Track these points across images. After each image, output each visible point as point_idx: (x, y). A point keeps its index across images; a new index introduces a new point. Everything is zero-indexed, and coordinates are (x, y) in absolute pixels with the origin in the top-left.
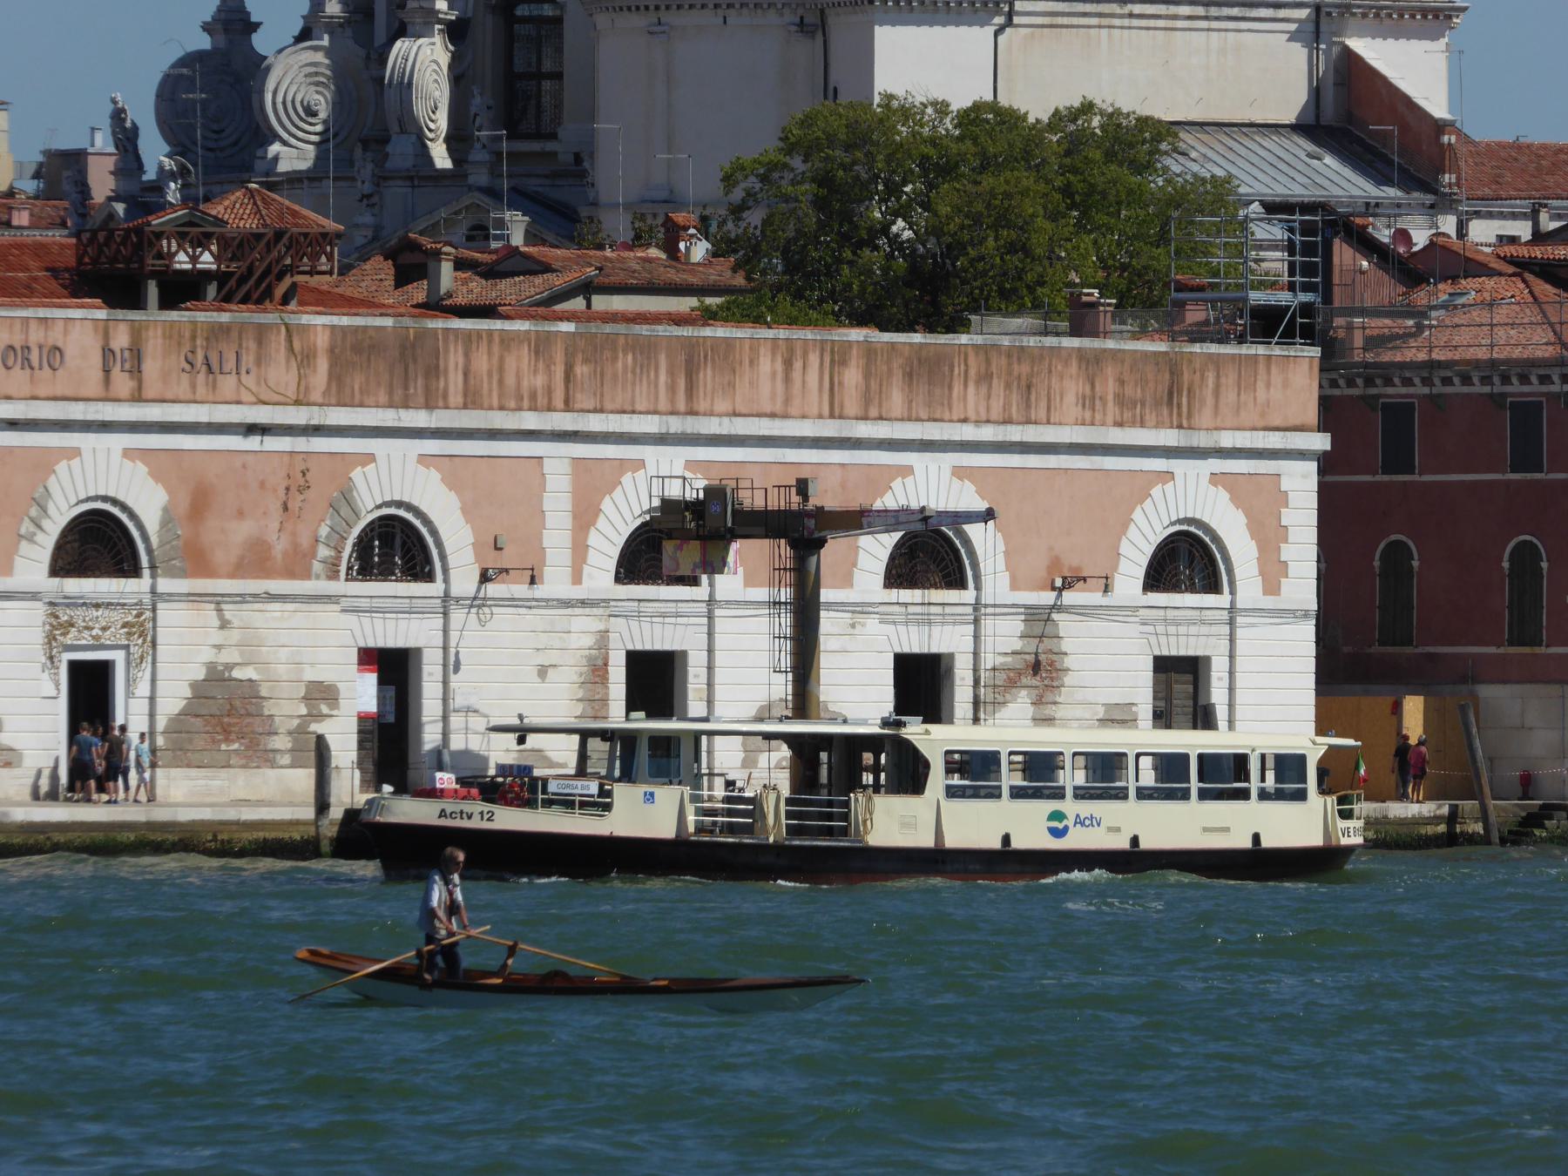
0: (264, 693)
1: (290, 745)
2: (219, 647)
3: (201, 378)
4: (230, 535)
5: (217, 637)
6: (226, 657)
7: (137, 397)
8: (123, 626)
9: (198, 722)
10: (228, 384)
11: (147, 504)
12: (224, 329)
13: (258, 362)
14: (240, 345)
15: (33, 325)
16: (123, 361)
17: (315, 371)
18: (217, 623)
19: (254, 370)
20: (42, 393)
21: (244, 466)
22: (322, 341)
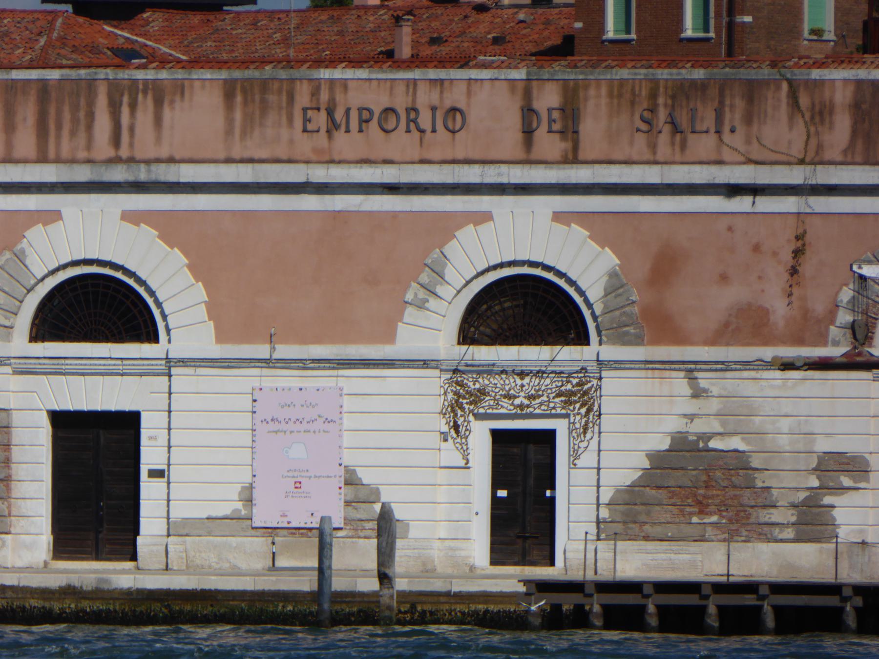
0: (755, 464)
1: (793, 519)
2: (691, 417)
3: (664, 138)
4: (706, 298)
5: (692, 407)
6: (699, 427)
7: (572, 158)
8: (559, 395)
9: (662, 494)
10: (704, 144)
11: (586, 267)
12: (701, 87)
13: (748, 119)
14: (722, 103)
15: (422, 89)
16: (551, 121)
17: (831, 127)
18: (688, 391)
19: (741, 129)
20: (436, 155)
21: (730, 229)
22: (842, 97)
